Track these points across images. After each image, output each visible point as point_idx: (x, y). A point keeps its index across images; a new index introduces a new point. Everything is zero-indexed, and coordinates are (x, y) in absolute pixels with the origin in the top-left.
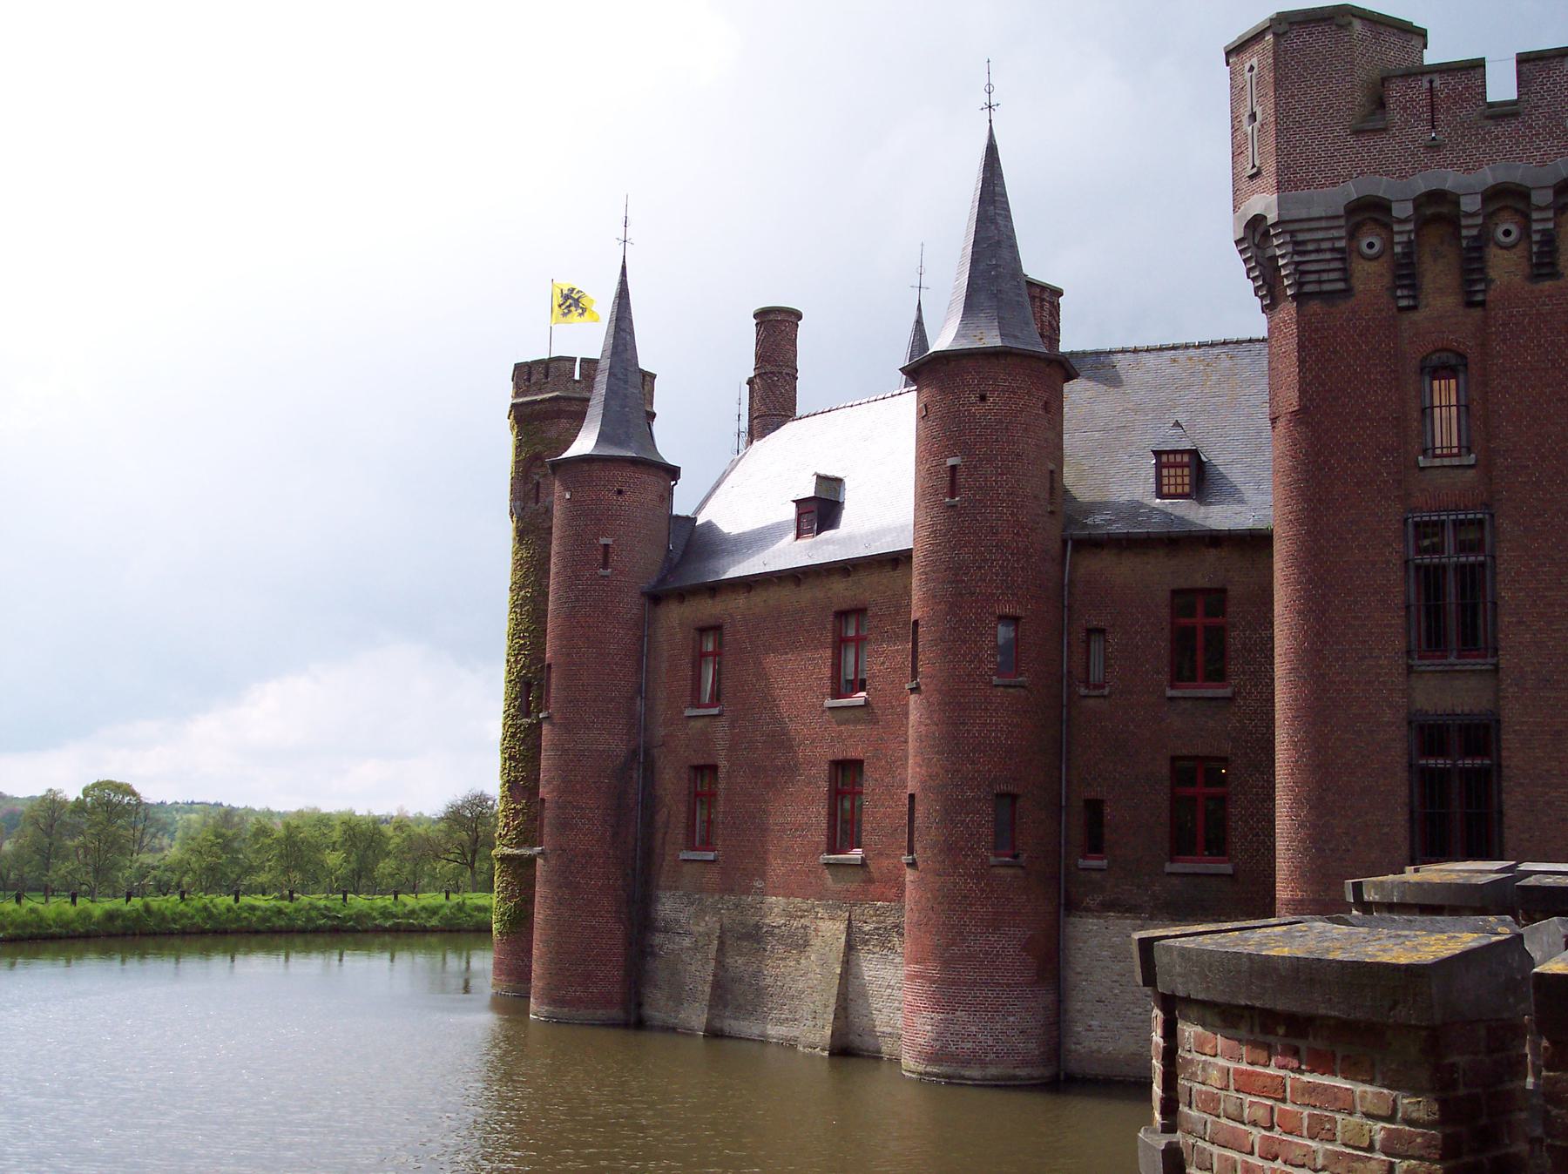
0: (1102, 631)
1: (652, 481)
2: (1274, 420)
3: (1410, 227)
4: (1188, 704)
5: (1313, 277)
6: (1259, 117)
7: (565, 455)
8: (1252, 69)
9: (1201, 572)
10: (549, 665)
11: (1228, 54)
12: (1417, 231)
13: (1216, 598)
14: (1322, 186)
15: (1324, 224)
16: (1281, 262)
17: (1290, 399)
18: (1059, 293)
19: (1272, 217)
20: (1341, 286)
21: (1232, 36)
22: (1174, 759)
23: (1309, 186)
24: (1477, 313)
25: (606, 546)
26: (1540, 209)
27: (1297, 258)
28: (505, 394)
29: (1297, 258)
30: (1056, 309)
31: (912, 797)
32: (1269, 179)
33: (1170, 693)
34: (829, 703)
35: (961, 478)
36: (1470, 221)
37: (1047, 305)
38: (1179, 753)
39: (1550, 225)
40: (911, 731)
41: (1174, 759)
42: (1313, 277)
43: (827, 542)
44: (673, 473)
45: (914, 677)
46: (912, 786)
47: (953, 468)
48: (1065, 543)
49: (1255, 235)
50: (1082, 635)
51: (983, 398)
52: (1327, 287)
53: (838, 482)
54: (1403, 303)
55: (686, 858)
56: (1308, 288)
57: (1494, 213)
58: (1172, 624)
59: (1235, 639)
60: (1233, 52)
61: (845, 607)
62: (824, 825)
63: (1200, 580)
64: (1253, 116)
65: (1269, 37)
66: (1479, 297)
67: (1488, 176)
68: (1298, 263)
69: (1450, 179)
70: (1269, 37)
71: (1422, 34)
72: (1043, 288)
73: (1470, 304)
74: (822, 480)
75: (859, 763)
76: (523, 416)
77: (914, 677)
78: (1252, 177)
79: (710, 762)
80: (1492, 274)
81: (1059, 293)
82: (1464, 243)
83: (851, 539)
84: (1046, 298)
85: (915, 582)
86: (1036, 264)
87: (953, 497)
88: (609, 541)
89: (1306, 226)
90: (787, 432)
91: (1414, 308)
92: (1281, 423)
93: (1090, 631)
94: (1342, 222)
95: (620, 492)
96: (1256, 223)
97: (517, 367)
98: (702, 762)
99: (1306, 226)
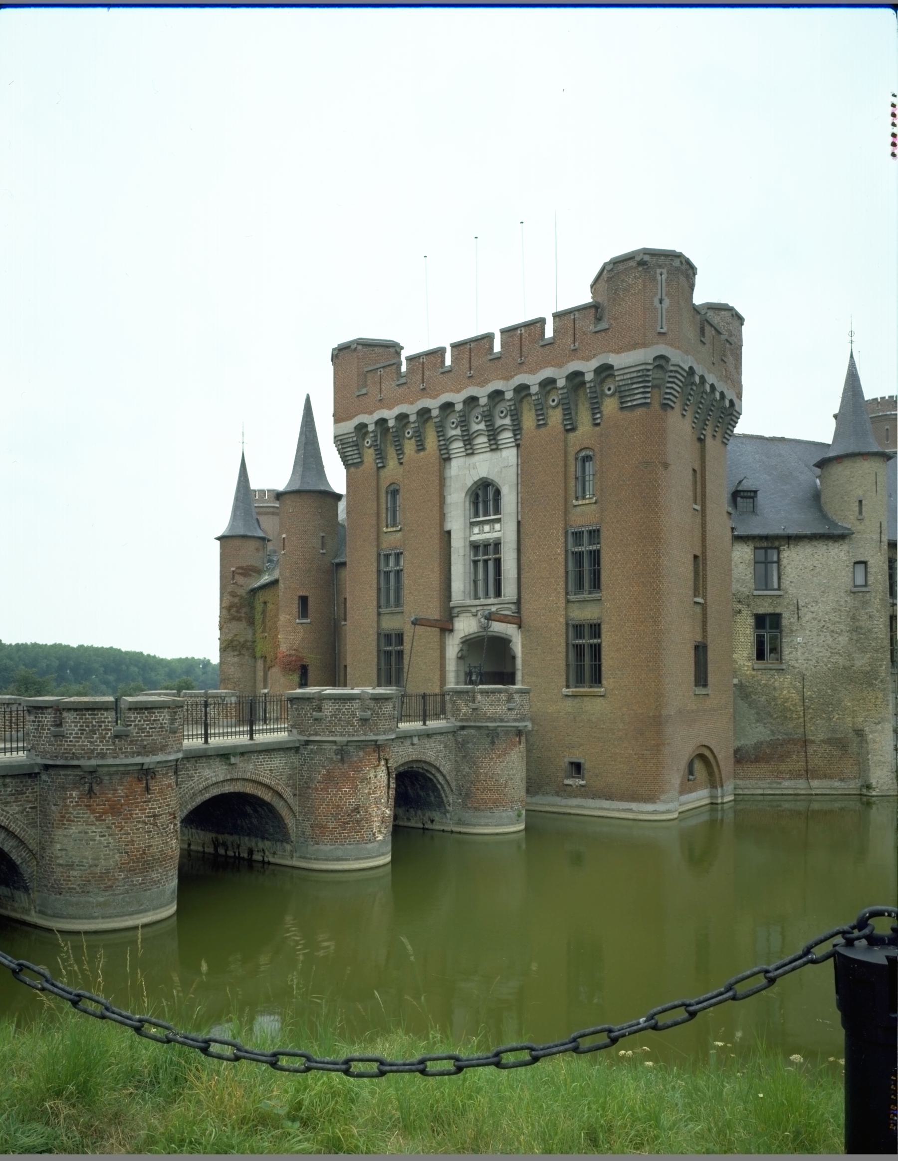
20: (359, 460)
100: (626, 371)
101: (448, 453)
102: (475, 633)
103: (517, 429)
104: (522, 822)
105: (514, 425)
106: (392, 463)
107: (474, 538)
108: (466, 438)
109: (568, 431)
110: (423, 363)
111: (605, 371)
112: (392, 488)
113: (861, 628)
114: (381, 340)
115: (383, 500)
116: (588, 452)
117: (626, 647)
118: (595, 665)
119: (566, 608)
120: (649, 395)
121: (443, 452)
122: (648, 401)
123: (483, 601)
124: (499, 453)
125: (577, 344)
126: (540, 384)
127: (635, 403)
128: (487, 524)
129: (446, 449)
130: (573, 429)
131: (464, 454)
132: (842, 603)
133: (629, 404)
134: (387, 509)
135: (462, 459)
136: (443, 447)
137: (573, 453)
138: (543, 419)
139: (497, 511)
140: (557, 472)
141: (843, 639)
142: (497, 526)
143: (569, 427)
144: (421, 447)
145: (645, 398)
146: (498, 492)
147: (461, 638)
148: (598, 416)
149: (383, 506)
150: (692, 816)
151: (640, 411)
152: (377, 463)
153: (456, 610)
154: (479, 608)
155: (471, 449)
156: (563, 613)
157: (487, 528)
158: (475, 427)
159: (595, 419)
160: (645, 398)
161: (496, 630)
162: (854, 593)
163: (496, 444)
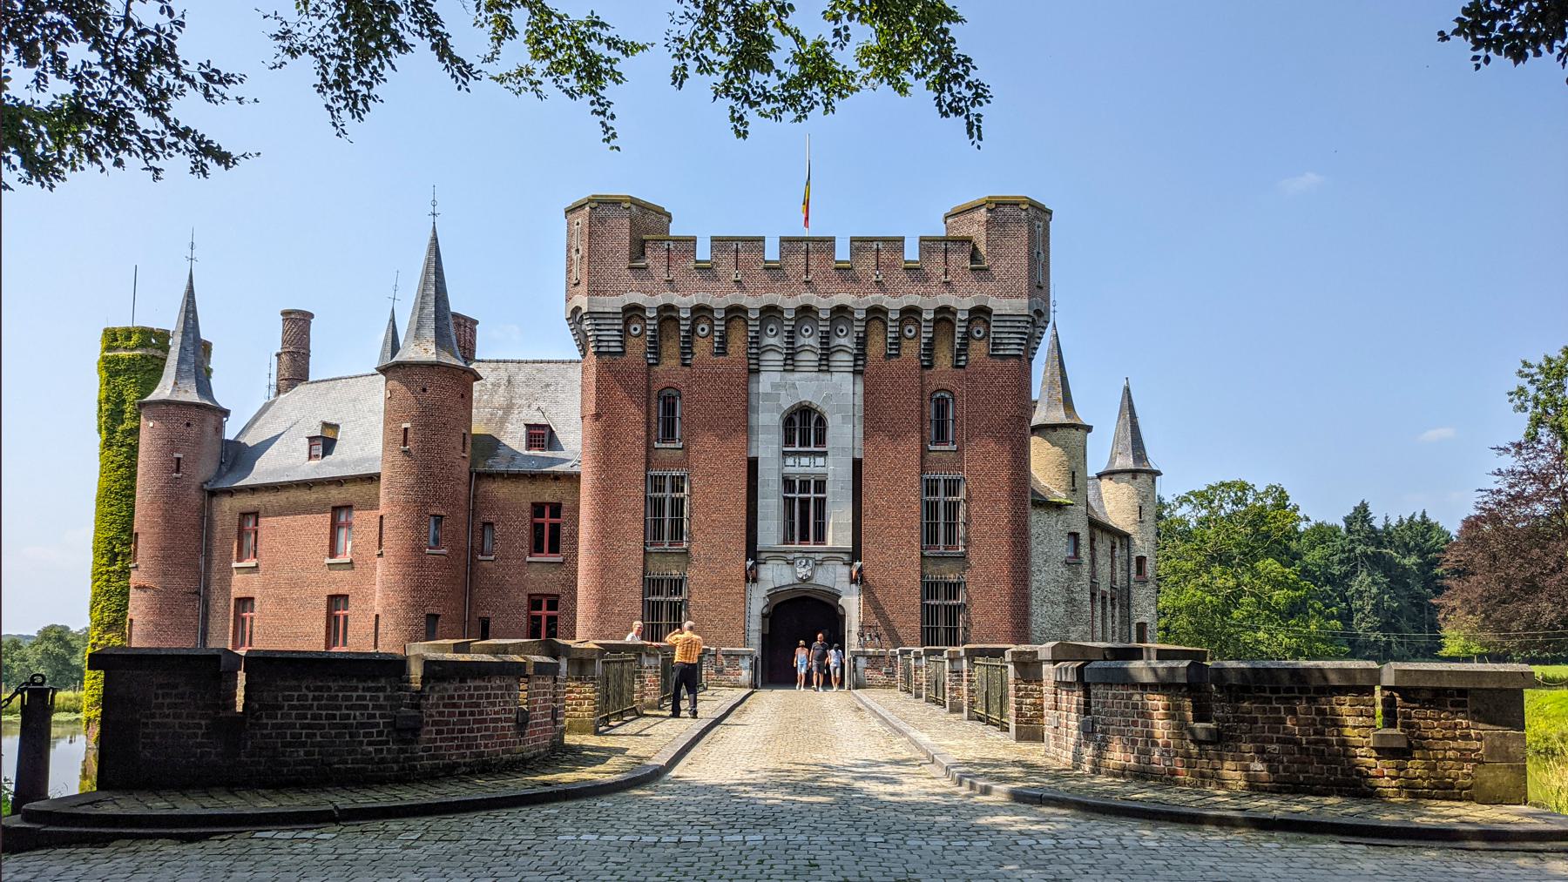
0: (492, 524)
1: (212, 420)
2: (582, 418)
3: (655, 322)
4: (538, 566)
5: (606, 344)
6: (581, 252)
7: (149, 398)
8: (578, 224)
9: (548, 494)
10: (137, 534)
11: (566, 212)
12: (660, 324)
13: (556, 509)
14: (612, 295)
15: (611, 316)
16: (589, 334)
17: (591, 408)
18: (476, 322)
19: (585, 309)
20: (620, 350)
21: (569, 204)
22: (530, 595)
23: (605, 294)
24: (687, 369)
25: (179, 459)
26: (718, 319)
27: (597, 333)
28: (94, 351)
29: (597, 333)
30: (473, 332)
31: (377, 616)
32: (583, 287)
33: (528, 559)
34: (328, 561)
35: (410, 436)
36: (684, 322)
37: (468, 330)
38: (533, 592)
39: (723, 328)
40: (378, 579)
41: (530, 595)
42: (606, 344)
43: (328, 464)
44: (226, 413)
45: (380, 548)
46: (378, 610)
47: (406, 429)
48: (471, 474)
49: (575, 316)
50: (481, 526)
51: (424, 390)
52: (611, 350)
53: (336, 427)
54: (651, 361)
55: (1088, 596)
56: (601, 349)
57: (697, 318)
58: (532, 521)
59: (565, 530)
60: (570, 211)
61: (339, 504)
62: (324, 634)
63: (548, 498)
64: (578, 250)
65: (587, 208)
66: (688, 362)
67: (694, 299)
68: (598, 336)
69: (676, 299)
70: (587, 208)
71: (669, 216)
72: (466, 319)
73: (684, 365)
74: (326, 425)
75: (346, 597)
76: (112, 369)
77: (380, 548)
78: (575, 285)
79: (250, 595)
80: (695, 350)
81: (476, 322)
82: (682, 334)
83: (343, 463)
84: (467, 325)
85: (382, 493)
86: (458, 304)
87: (405, 445)
88: (181, 456)
89: (601, 316)
90: (301, 388)
91: (657, 364)
92: (587, 420)
93: (485, 524)
94: (621, 316)
95: (188, 425)
96: (577, 310)
97: (106, 330)
98: (243, 595)
99: (601, 316)
100: (1007, 318)
101: (758, 364)
102: (789, 585)
103: (861, 353)
104: (13, 734)
105: (858, 349)
106: (670, 362)
107: (788, 470)
108: (790, 351)
109: (923, 367)
110: (878, 250)
111: (980, 313)
112: (665, 393)
113: (1075, 600)
114: (1008, 197)
115: (654, 405)
116: (943, 394)
117: (995, 610)
118: (928, 628)
119: (922, 565)
120: (1023, 348)
121: (752, 361)
122: (1021, 353)
123: (811, 546)
124: (828, 376)
125: (949, 277)
126: (971, 311)
127: (1007, 353)
128: (806, 456)
129: (757, 359)
130: (930, 367)
131: (782, 369)
132: (1059, 574)
133: (1001, 352)
134: (658, 418)
135: (779, 374)
136: (754, 356)
137: (656, 393)
138: (896, 349)
139: (821, 440)
140: (913, 411)
141: (1061, 610)
142: (820, 461)
143: (926, 363)
144: (722, 350)
145: (1019, 350)
146: (821, 421)
147: (769, 591)
148: (964, 358)
149: (654, 415)
150: (1558, 851)
151: (1012, 362)
152: (922, 361)
153: (763, 556)
154: (797, 555)
155: (792, 365)
156: (919, 568)
157: (805, 461)
158: (769, 341)
159: (958, 361)
160: (1019, 350)
161: (819, 582)
162: (1069, 564)
163: (828, 365)
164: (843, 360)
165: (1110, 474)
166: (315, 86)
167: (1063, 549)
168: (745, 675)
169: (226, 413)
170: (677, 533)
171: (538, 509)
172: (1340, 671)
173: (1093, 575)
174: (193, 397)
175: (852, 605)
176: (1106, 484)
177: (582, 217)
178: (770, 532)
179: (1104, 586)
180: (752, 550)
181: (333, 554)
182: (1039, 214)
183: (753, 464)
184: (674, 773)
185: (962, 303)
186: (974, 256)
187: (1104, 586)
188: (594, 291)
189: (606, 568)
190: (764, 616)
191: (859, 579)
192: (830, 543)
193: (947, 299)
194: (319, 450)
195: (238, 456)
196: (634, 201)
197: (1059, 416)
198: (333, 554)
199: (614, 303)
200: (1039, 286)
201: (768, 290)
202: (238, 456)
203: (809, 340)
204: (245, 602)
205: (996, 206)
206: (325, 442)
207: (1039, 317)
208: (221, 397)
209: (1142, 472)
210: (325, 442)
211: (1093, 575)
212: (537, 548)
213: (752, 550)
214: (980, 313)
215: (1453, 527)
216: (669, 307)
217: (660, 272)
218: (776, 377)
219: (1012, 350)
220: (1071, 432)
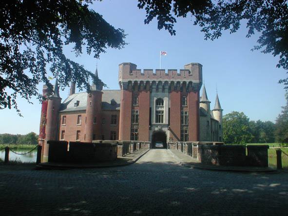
13: (116, 116)
44: (61, 99)
67: (140, 80)
96: (120, 82)
123: (161, 123)
126: (152, 82)
164: (167, 90)
165: (215, 110)
166: (231, 33)
167: (206, 123)
168: (149, 146)
169: (61, 99)
170: (137, 121)
171: (113, 116)
172: (207, 144)
173: (211, 128)
174: (57, 97)
175: (168, 133)
176: (214, 112)
177: (121, 66)
178: (154, 122)
179: (214, 130)
180: (150, 124)
181: (78, 123)
182: (200, 66)
183: (150, 109)
184: (137, 162)
185: (188, 81)
186: (190, 72)
187: (214, 130)
188: (123, 79)
189: (124, 127)
190: (152, 136)
191: (170, 129)
192: (164, 123)
193: (185, 80)
194: (76, 105)
195: (64, 106)
196: (130, 63)
197: (205, 100)
198: (78, 123)
199: (127, 81)
200: (201, 77)
201: (153, 78)
202: (64, 106)
203: (160, 87)
204: (63, 131)
205: (193, 65)
206: (78, 103)
207: (200, 84)
208: (61, 97)
209: (220, 110)
210: (78, 103)
211: (211, 128)
212: (112, 123)
213: (150, 124)
214: (190, 83)
215: (275, 122)
216: (185, 82)
217: (135, 75)
218: (155, 93)
219: (196, 89)
220: (208, 103)
